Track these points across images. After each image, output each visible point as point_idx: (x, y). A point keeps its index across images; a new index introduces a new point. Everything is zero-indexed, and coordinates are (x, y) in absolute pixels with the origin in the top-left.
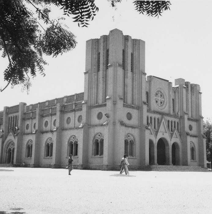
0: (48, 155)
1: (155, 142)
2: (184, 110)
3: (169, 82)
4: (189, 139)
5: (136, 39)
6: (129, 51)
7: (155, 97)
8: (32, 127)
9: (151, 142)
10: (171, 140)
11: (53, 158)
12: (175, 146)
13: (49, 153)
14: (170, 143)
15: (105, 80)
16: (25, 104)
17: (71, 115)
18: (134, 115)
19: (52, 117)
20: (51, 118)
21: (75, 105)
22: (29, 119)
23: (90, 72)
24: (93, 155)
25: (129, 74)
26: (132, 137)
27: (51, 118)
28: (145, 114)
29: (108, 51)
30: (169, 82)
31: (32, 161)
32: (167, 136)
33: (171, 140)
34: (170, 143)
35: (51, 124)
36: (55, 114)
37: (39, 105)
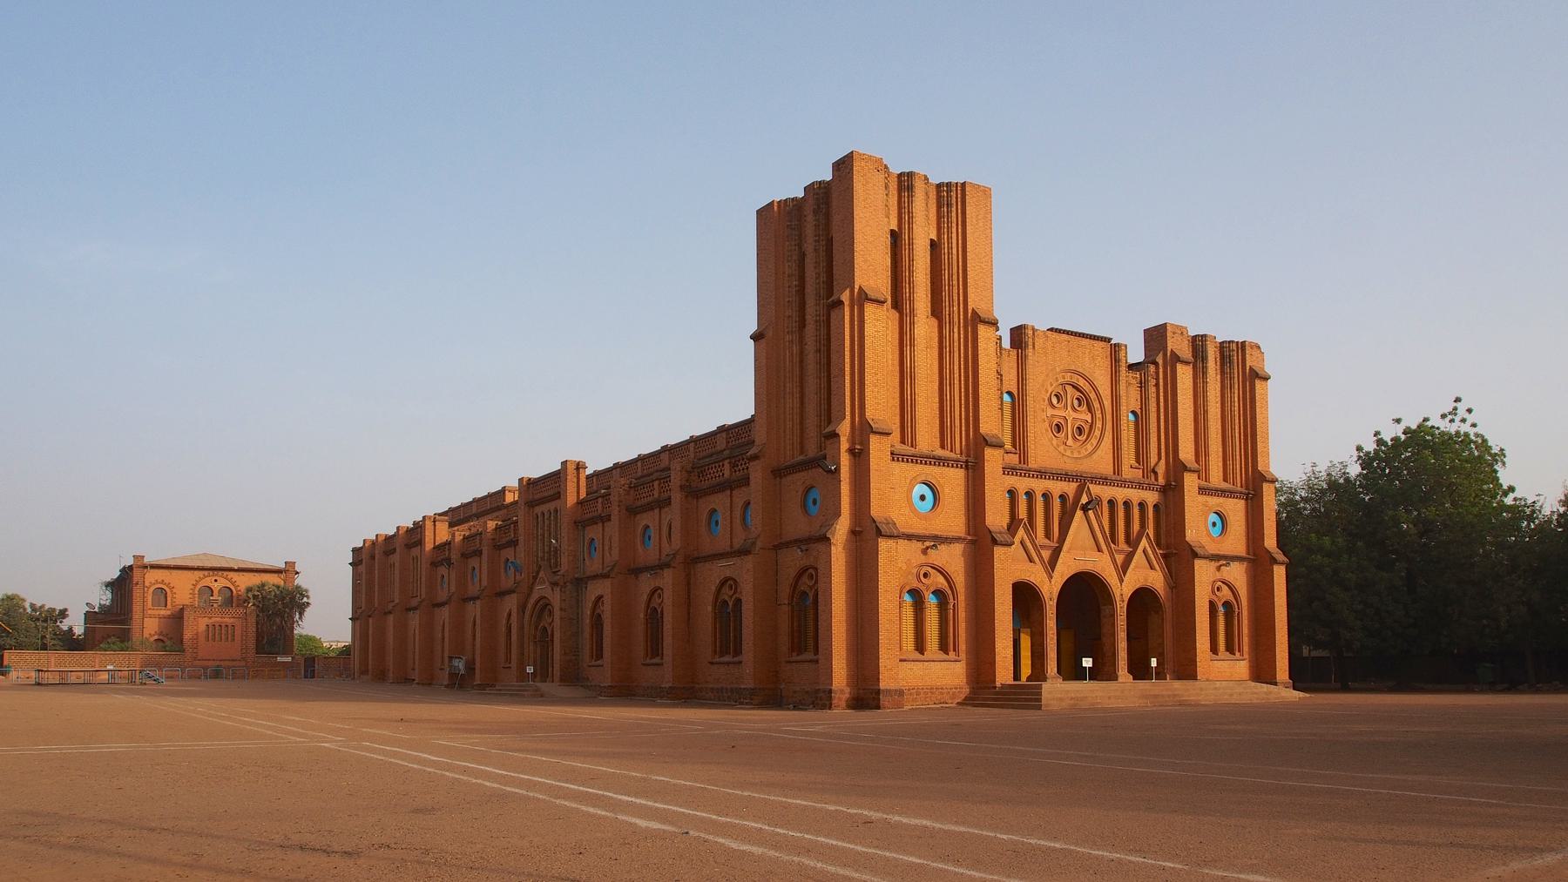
0: (724, 651)
1: (1050, 589)
2: (1182, 456)
3: (1113, 342)
4: (1204, 573)
5: (949, 185)
6: (923, 232)
7: (1050, 412)
8: (603, 550)
9: (1025, 596)
10: (1121, 581)
11: (665, 665)
12: (1142, 599)
13: (728, 641)
14: (1122, 590)
15: (824, 361)
16: (579, 466)
17: (719, 501)
18: (947, 490)
19: (663, 511)
20: (660, 514)
21: (730, 463)
22: (649, 507)
23: (770, 334)
24: (793, 651)
25: (924, 328)
26: (941, 579)
27: (660, 514)
28: (996, 486)
29: (830, 242)
30: (1113, 342)
31: (666, 675)
32: (1102, 565)
33: (1121, 581)
34: (1122, 590)
35: (660, 539)
36: (668, 502)
37: (639, 464)
